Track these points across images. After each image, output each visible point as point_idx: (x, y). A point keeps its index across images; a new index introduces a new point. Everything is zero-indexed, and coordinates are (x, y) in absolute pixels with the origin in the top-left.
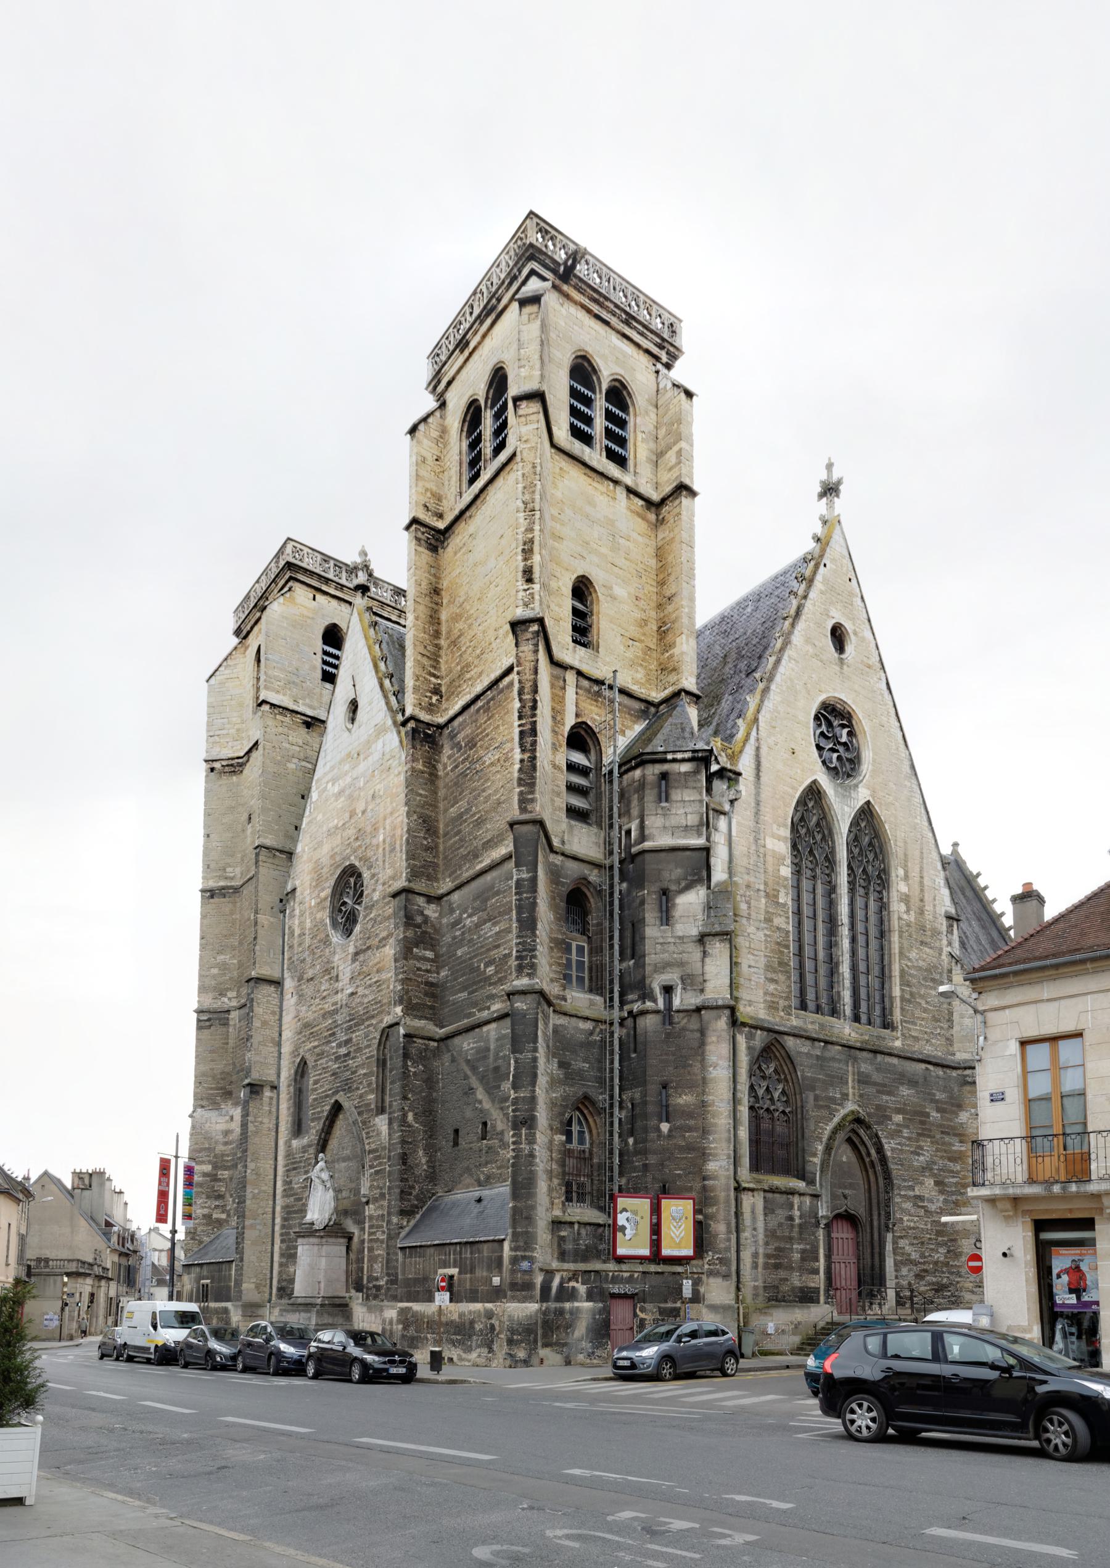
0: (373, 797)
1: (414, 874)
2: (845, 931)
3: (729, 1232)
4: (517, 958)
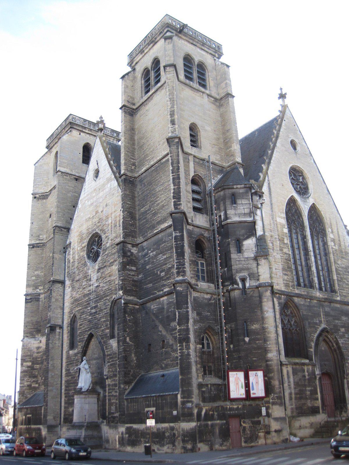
0: (106, 205)
1: (126, 235)
2: (312, 253)
3: (280, 384)
4: (177, 269)
